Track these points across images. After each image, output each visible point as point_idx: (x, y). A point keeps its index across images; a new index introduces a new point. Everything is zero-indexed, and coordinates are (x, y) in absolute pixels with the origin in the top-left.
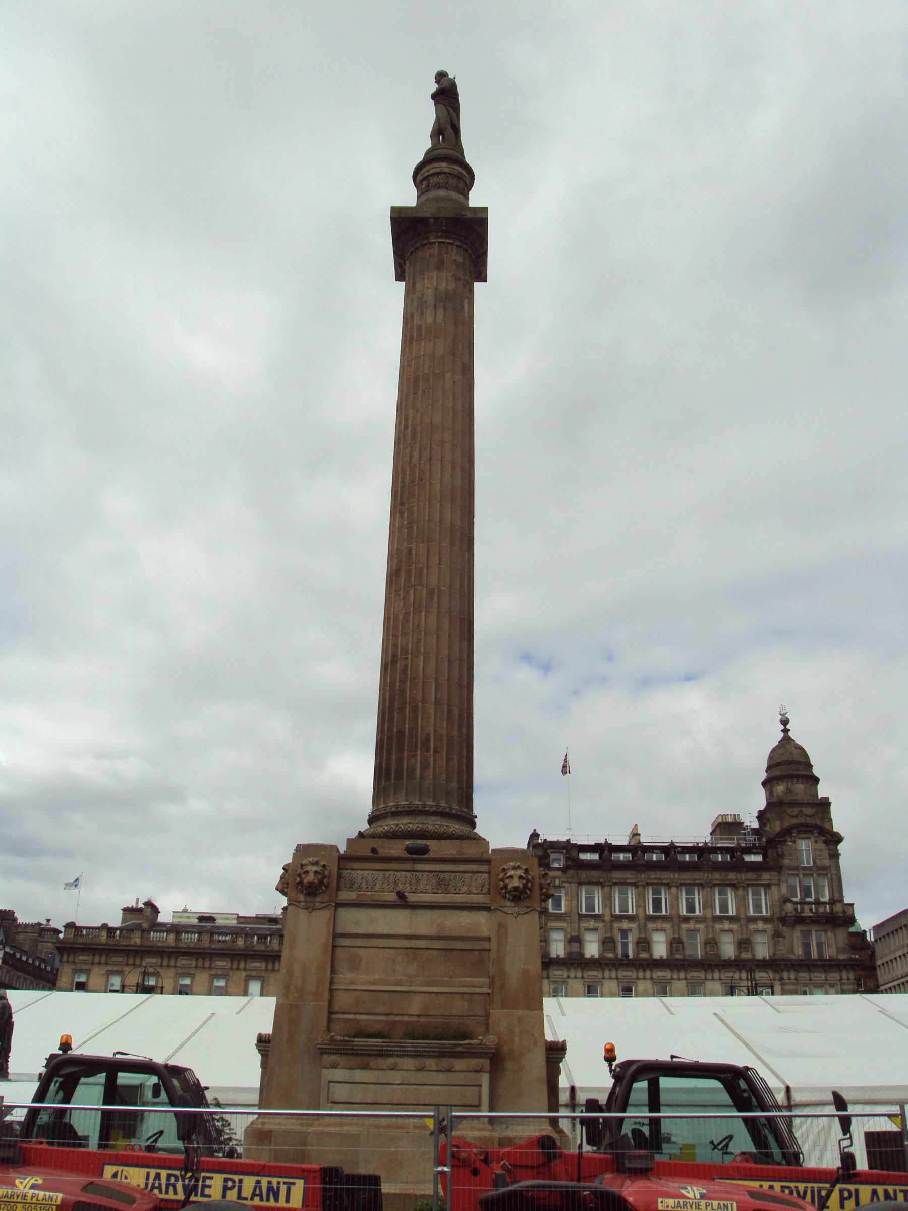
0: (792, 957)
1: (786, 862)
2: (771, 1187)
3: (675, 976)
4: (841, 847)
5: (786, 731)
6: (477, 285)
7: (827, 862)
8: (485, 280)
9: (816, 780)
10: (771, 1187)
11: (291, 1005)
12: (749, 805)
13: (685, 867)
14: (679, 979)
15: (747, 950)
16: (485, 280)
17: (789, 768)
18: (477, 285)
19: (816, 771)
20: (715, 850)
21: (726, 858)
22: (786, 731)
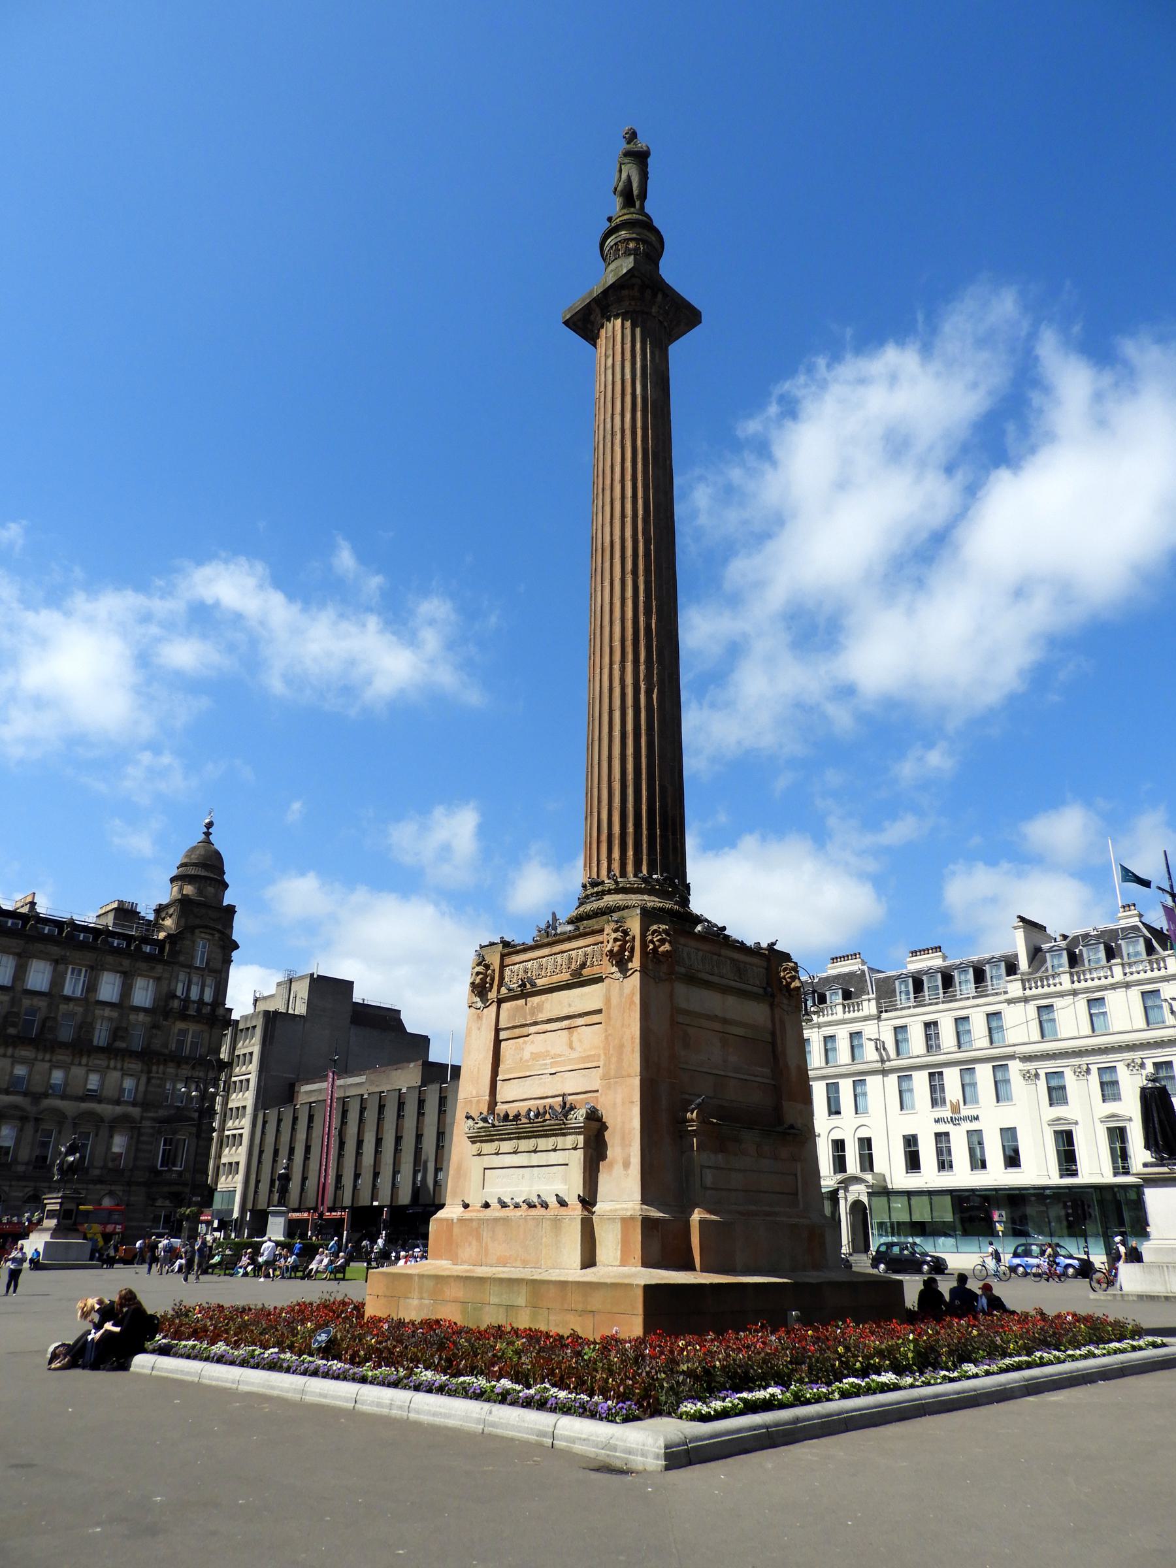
0: (166, 1051)
1: (182, 959)
2: (236, 1140)
3: (40, 1057)
4: (235, 954)
5: (207, 834)
6: (357, 997)
7: (217, 965)
8: (350, 984)
9: (226, 886)
10: (236, 1140)
11: (845, 998)
12: (153, 892)
13: (83, 946)
14: (43, 1060)
15: (123, 1039)
16: (350, 984)
17: (205, 873)
18: (357, 997)
19: (227, 878)
20: (113, 934)
21: (122, 940)
22: (207, 834)
